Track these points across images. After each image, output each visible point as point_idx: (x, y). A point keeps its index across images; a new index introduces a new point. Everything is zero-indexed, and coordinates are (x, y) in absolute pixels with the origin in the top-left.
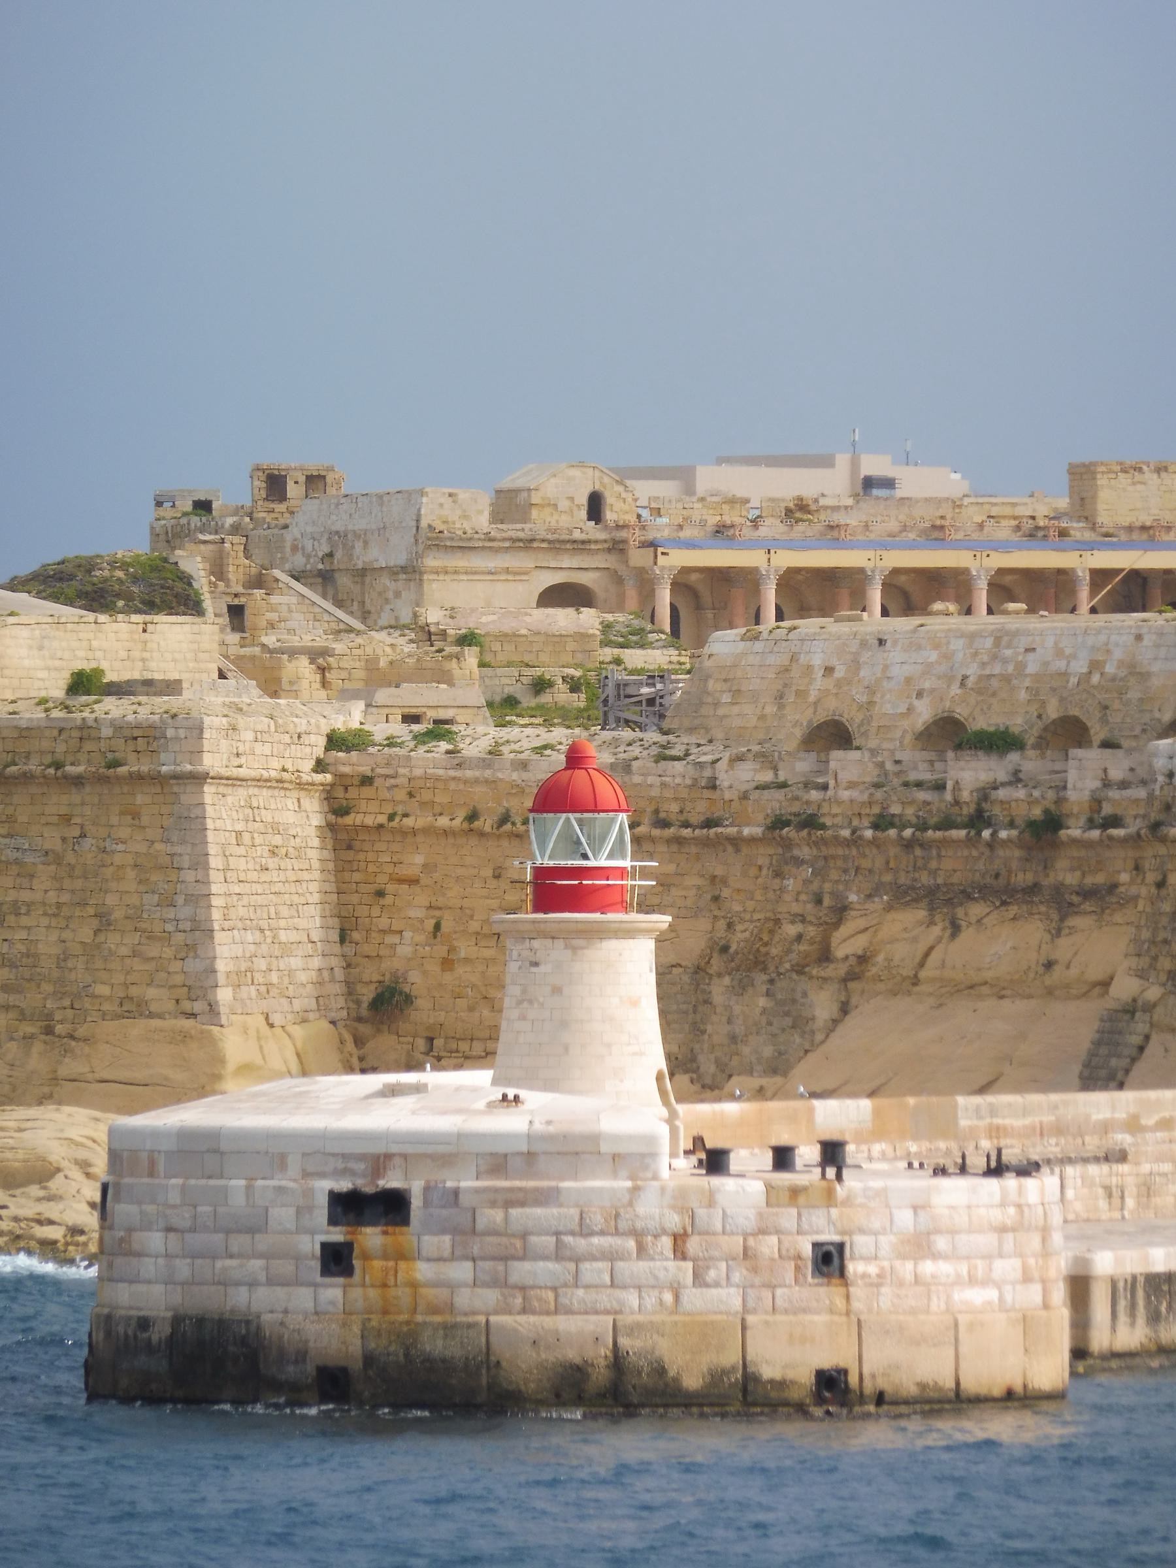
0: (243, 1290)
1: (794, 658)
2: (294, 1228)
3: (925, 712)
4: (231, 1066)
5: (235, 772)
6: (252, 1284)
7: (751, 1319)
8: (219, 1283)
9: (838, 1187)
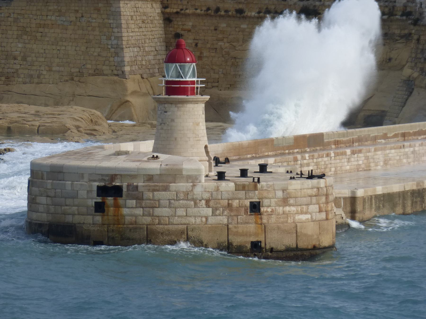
0: (71, 217)
2: (86, 197)
4: (129, 92)
6: (73, 215)
7: (230, 226)
8: (63, 214)
9: (258, 185)
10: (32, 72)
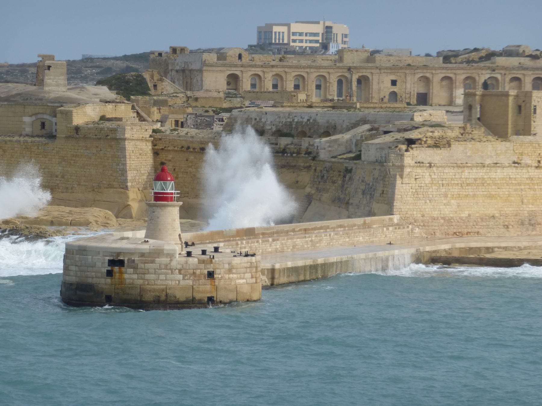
3: (274, 129)
5: (132, 138)
6: (93, 278)
7: (194, 287)
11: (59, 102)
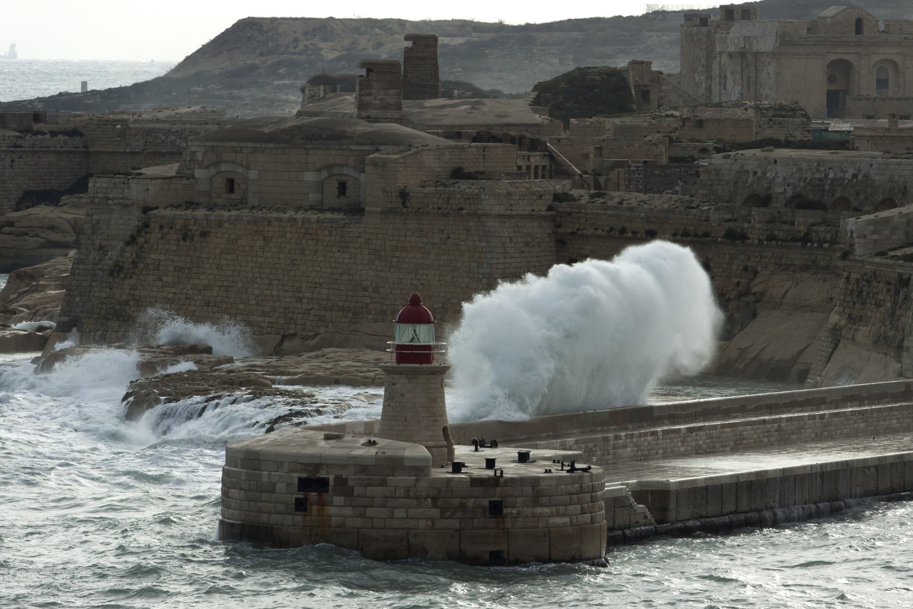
1: (742, 167)
3: (790, 193)
10: (385, 308)
11: (373, 143)
